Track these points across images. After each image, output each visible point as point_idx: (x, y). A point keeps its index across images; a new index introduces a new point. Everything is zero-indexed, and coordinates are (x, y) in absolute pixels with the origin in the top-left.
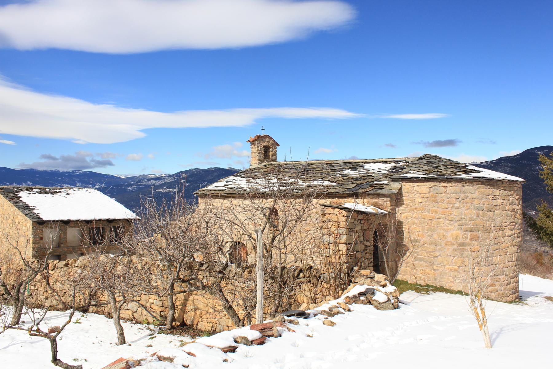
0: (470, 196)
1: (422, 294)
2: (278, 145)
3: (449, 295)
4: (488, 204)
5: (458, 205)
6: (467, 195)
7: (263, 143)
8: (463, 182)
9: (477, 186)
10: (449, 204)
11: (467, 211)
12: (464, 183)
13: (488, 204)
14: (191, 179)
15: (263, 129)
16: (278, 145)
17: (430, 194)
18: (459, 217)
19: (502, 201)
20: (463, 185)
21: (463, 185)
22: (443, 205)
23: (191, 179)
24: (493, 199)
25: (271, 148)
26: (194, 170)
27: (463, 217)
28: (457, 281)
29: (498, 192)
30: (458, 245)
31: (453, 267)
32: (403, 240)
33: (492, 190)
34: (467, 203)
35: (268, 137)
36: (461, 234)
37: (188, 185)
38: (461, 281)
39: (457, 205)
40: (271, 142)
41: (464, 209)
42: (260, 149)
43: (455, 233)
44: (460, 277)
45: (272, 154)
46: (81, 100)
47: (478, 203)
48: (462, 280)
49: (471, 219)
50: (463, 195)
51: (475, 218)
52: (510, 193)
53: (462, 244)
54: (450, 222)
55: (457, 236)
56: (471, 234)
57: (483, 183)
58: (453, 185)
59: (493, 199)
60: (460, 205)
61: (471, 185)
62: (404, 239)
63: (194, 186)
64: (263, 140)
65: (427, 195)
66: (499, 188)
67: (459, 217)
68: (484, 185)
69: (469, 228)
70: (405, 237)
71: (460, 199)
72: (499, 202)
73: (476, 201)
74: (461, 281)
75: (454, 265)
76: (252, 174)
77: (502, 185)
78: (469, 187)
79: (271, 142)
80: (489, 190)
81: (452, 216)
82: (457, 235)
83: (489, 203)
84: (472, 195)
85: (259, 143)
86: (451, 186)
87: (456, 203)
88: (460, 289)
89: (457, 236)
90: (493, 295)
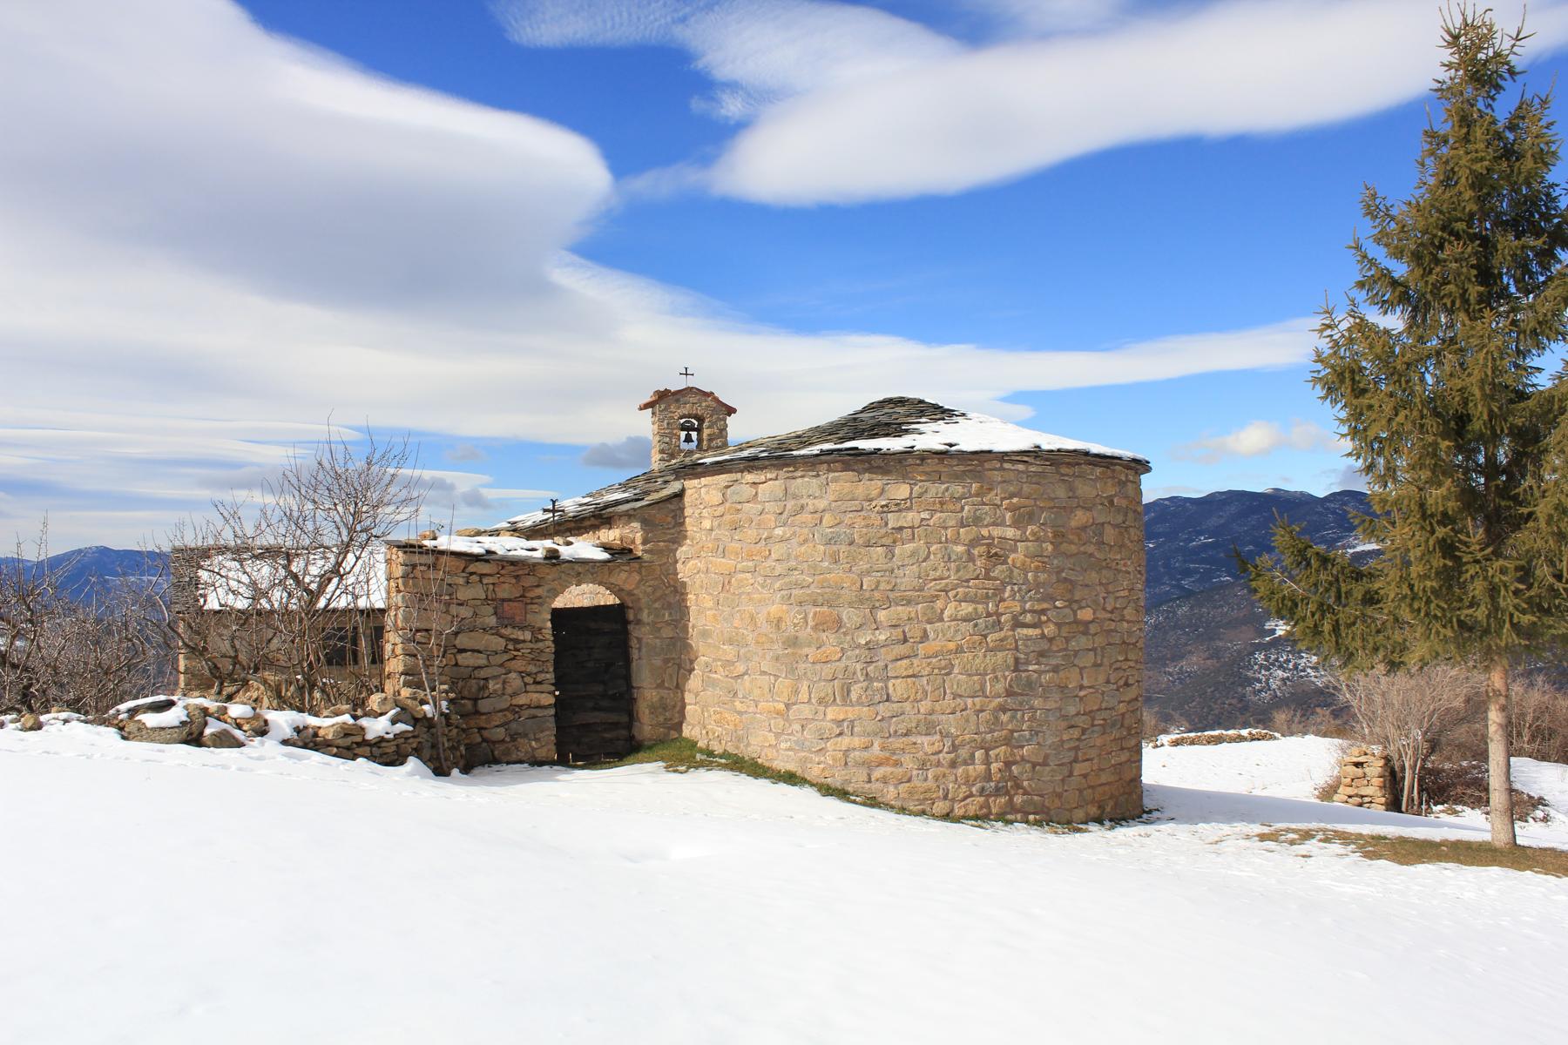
0: (811, 504)
1: (1536, 872)
2: (731, 411)
3: (763, 784)
4: (867, 526)
5: (781, 533)
6: (803, 501)
7: (679, 408)
8: (788, 465)
9: (831, 475)
10: (761, 531)
11: (803, 549)
12: (792, 469)
13: (867, 526)
14: (1160, 528)
15: (686, 374)
16: (731, 411)
17: (727, 505)
18: (786, 565)
19: (925, 515)
20: (790, 475)
21: (790, 475)
22: (750, 532)
23: (1160, 528)
24: (885, 509)
25: (707, 420)
26: (1166, 502)
27: (793, 563)
28: (783, 745)
29: (901, 491)
30: (783, 643)
31: (776, 704)
32: (688, 632)
33: (879, 483)
34: (803, 525)
35: (696, 394)
36: (792, 616)
37: (1151, 546)
38: (793, 745)
39: (779, 531)
40: (704, 404)
41: (794, 541)
42: (668, 424)
43: (774, 609)
44: (792, 734)
45: (709, 435)
46: (900, 338)
47: (831, 523)
48: (796, 742)
49: (814, 570)
50: (793, 502)
51: (827, 568)
52: (958, 489)
53: (793, 642)
54: (765, 581)
55: (780, 620)
56: (815, 614)
57: (847, 467)
58: (769, 476)
59: (885, 509)
60: (784, 532)
61: (811, 473)
62: (690, 630)
63: (1169, 547)
64: (677, 401)
65: (721, 510)
66: (905, 477)
67: (786, 565)
68: (853, 470)
69: (808, 595)
70: (690, 625)
71: (785, 516)
72: (911, 517)
73: (828, 519)
74: (793, 745)
75: (777, 701)
76: (633, 485)
77: (921, 469)
78: (806, 479)
79: (704, 404)
80: (871, 485)
81: (770, 563)
82: (780, 614)
83: (871, 522)
84: (816, 501)
85: (665, 409)
86: (764, 480)
87: (776, 527)
88: (791, 767)
89: (780, 620)
90: (890, 793)
